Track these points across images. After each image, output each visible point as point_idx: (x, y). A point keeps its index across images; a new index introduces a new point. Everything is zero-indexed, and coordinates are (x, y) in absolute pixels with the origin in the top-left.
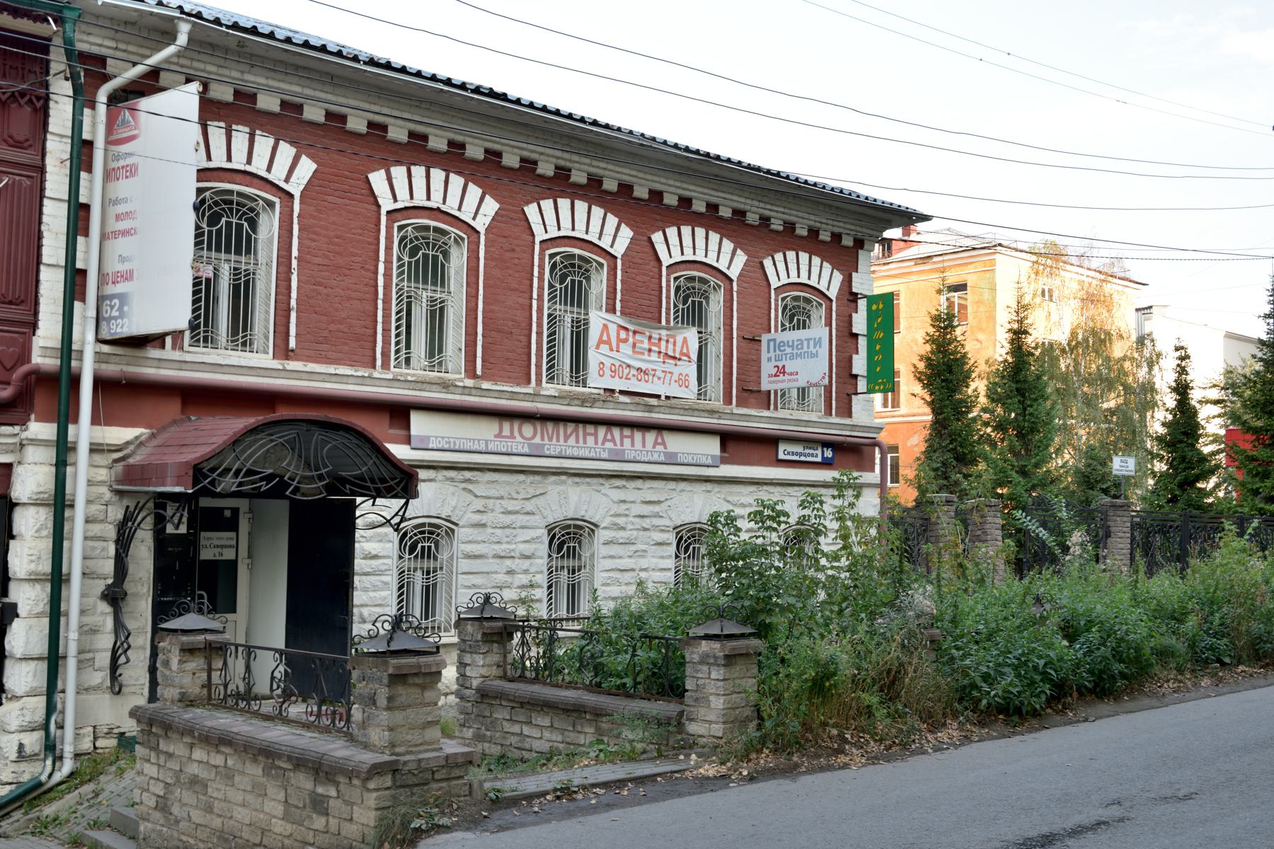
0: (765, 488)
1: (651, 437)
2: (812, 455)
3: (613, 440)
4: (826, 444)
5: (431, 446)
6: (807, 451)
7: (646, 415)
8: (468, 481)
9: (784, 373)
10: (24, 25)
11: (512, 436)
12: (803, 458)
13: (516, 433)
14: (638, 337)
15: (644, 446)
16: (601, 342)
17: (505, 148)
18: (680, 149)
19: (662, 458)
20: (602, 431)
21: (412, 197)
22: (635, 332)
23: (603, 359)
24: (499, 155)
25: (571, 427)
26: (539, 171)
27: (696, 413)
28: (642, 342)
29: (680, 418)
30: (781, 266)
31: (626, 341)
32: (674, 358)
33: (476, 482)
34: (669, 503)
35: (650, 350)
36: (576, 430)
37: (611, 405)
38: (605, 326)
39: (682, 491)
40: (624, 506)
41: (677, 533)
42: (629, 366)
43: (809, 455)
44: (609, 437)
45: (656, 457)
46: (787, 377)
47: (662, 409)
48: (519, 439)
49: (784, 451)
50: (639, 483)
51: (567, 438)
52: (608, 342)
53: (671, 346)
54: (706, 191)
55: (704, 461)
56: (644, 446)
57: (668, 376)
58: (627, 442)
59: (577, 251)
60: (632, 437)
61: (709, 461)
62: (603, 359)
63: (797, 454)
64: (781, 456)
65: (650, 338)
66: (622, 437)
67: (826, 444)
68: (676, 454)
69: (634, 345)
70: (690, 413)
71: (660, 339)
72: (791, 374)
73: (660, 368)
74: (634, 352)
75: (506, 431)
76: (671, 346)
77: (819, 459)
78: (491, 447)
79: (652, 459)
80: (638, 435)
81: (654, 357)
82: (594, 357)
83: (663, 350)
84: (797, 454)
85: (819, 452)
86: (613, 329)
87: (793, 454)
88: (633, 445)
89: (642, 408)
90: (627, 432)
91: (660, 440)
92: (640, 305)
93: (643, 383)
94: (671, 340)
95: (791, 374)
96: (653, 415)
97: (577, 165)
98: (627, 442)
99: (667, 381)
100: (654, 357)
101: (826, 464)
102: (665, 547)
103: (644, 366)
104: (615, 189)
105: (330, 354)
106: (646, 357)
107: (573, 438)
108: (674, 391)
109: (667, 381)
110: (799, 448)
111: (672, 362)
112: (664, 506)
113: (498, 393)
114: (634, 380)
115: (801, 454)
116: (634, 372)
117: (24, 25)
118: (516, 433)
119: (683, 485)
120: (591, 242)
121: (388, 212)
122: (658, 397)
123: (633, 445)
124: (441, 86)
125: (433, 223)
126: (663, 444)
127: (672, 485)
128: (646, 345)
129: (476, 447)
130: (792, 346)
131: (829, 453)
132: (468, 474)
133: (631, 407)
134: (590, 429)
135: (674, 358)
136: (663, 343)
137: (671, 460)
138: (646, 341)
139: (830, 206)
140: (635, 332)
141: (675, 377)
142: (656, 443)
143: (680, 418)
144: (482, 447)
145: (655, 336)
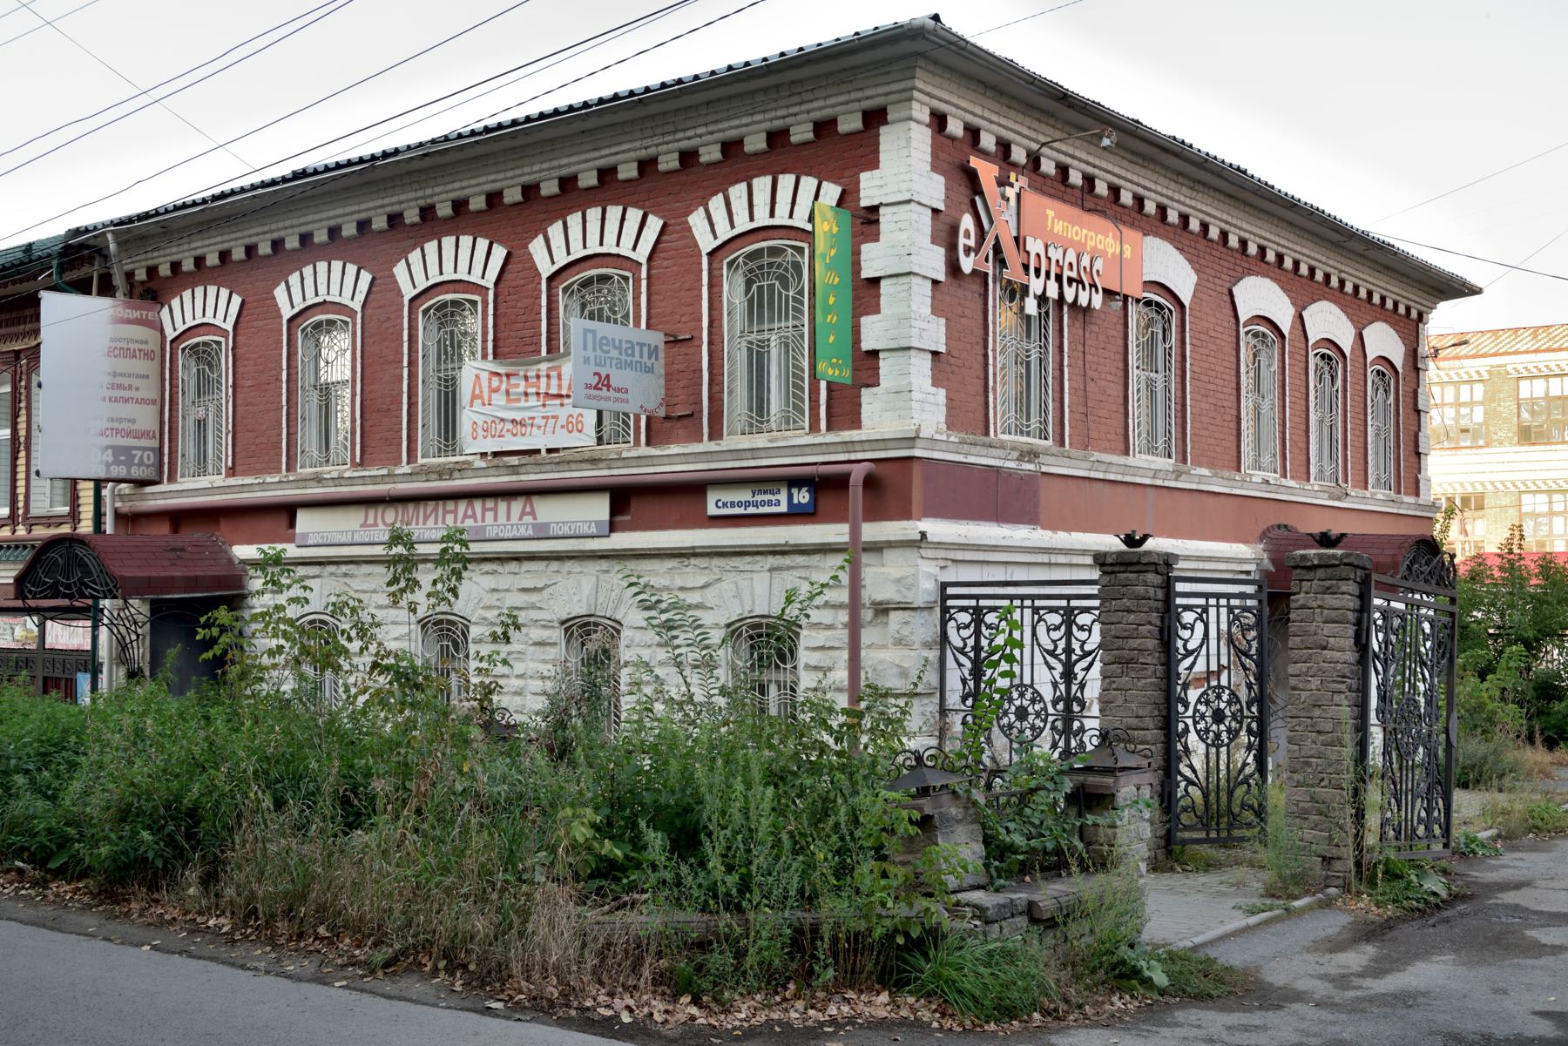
0: (693, 561)
1: (517, 505)
2: (770, 503)
3: (474, 516)
4: (794, 482)
5: (310, 542)
6: (759, 498)
7: (514, 478)
8: (345, 575)
9: (608, 386)
10: (18, 288)
11: (375, 524)
12: (751, 510)
13: (379, 521)
14: (513, 380)
15: (509, 518)
16: (474, 397)
17: (370, 213)
18: (480, 134)
19: (530, 533)
20: (462, 506)
21: (791, 216)
22: (508, 376)
23: (476, 418)
24: (573, 178)
25: (431, 504)
26: (407, 221)
27: (574, 466)
28: (518, 386)
29: (556, 476)
30: (322, 278)
31: (496, 390)
32: (560, 396)
33: (352, 576)
34: (549, 590)
35: (526, 394)
36: (436, 510)
37: (470, 473)
38: (477, 376)
39: (569, 573)
40: (496, 596)
41: (566, 630)
42: (502, 420)
43: (763, 503)
44: (528, 509)
45: (522, 532)
46: (612, 394)
47: (529, 468)
48: (381, 526)
49: (715, 503)
50: (513, 566)
51: (426, 519)
52: (480, 397)
53: (554, 382)
54: (583, 157)
55: (585, 530)
56: (509, 518)
57: (551, 421)
58: (489, 515)
59: (449, 297)
60: (495, 510)
61: (593, 530)
62: (476, 418)
63: (740, 504)
64: (712, 510)
65: (526, 378)
66: (484, 510)
67: (794, 482)
68: (548, 524)
69: (508, 392)
70: (566, 467)
71: (538, 377)
72: (619, 390)
73: (538, 414)
74: (508, 401)
75: (371, 521)
76: (554, 382)
77: (783, 508)
78: (357, 539)
79: (518, 535)
80: (502, 506)
81: (533, 401)
82: (468, 418)
83: (542, 390)
84: (740, 504)
85: (783, 497)
86: (485, 376)
87: (733, 505)
88: (496, 519)
89: (504, 471)
90: (490, 503)
91: (528, 509)
92: (519, 339)
93: (519, 439)
94: (554, 374)
95: (619, 390)
96: (523, 477)
97: (436, 198)
98: (489, 515)
99: (549, 429)
100: (533, 401)
101: (796, 515)
102: (548, 648)
103: (518, 416)
104: (810, 136)
105: (258, 466)
106: (523, 404)
107: (432, 519)
108: (562, 440)
109: (549, 429)
110: (744, 495)
111: (558, 402)
112: (545, 593)
113: (372, 480)
114: (508, 436)
115: (747, 504)
116: (509, 426)
117: (18, 288)
118: (379, 521)
119: (569, 565)
120: (609, 255)
121: (710, 254)
122: (538, 451)
123: (496, 519)
124: (260, 191)
125: (764, 244)
126: (533, 513)
127: (554, 565)
128: (521, 390)
129: (344, 540)
130: (620, 348)
131: (803, 497)
132: (344, 568)
133: (492, 471)
134: (450, 505)
135: (560, 396)
136: (543, 380)
137: (542, 534)
138: (523, 383)
139: (777, 87)
140: (508, 376)
141: (562, 421)
142: (523, 513)
143: (333, 490)
144: (348, 539)
145: (531, 374)
